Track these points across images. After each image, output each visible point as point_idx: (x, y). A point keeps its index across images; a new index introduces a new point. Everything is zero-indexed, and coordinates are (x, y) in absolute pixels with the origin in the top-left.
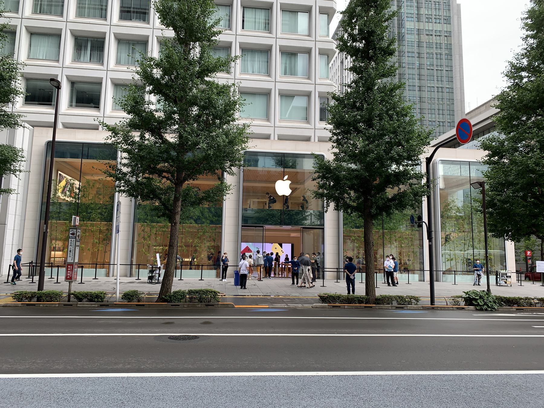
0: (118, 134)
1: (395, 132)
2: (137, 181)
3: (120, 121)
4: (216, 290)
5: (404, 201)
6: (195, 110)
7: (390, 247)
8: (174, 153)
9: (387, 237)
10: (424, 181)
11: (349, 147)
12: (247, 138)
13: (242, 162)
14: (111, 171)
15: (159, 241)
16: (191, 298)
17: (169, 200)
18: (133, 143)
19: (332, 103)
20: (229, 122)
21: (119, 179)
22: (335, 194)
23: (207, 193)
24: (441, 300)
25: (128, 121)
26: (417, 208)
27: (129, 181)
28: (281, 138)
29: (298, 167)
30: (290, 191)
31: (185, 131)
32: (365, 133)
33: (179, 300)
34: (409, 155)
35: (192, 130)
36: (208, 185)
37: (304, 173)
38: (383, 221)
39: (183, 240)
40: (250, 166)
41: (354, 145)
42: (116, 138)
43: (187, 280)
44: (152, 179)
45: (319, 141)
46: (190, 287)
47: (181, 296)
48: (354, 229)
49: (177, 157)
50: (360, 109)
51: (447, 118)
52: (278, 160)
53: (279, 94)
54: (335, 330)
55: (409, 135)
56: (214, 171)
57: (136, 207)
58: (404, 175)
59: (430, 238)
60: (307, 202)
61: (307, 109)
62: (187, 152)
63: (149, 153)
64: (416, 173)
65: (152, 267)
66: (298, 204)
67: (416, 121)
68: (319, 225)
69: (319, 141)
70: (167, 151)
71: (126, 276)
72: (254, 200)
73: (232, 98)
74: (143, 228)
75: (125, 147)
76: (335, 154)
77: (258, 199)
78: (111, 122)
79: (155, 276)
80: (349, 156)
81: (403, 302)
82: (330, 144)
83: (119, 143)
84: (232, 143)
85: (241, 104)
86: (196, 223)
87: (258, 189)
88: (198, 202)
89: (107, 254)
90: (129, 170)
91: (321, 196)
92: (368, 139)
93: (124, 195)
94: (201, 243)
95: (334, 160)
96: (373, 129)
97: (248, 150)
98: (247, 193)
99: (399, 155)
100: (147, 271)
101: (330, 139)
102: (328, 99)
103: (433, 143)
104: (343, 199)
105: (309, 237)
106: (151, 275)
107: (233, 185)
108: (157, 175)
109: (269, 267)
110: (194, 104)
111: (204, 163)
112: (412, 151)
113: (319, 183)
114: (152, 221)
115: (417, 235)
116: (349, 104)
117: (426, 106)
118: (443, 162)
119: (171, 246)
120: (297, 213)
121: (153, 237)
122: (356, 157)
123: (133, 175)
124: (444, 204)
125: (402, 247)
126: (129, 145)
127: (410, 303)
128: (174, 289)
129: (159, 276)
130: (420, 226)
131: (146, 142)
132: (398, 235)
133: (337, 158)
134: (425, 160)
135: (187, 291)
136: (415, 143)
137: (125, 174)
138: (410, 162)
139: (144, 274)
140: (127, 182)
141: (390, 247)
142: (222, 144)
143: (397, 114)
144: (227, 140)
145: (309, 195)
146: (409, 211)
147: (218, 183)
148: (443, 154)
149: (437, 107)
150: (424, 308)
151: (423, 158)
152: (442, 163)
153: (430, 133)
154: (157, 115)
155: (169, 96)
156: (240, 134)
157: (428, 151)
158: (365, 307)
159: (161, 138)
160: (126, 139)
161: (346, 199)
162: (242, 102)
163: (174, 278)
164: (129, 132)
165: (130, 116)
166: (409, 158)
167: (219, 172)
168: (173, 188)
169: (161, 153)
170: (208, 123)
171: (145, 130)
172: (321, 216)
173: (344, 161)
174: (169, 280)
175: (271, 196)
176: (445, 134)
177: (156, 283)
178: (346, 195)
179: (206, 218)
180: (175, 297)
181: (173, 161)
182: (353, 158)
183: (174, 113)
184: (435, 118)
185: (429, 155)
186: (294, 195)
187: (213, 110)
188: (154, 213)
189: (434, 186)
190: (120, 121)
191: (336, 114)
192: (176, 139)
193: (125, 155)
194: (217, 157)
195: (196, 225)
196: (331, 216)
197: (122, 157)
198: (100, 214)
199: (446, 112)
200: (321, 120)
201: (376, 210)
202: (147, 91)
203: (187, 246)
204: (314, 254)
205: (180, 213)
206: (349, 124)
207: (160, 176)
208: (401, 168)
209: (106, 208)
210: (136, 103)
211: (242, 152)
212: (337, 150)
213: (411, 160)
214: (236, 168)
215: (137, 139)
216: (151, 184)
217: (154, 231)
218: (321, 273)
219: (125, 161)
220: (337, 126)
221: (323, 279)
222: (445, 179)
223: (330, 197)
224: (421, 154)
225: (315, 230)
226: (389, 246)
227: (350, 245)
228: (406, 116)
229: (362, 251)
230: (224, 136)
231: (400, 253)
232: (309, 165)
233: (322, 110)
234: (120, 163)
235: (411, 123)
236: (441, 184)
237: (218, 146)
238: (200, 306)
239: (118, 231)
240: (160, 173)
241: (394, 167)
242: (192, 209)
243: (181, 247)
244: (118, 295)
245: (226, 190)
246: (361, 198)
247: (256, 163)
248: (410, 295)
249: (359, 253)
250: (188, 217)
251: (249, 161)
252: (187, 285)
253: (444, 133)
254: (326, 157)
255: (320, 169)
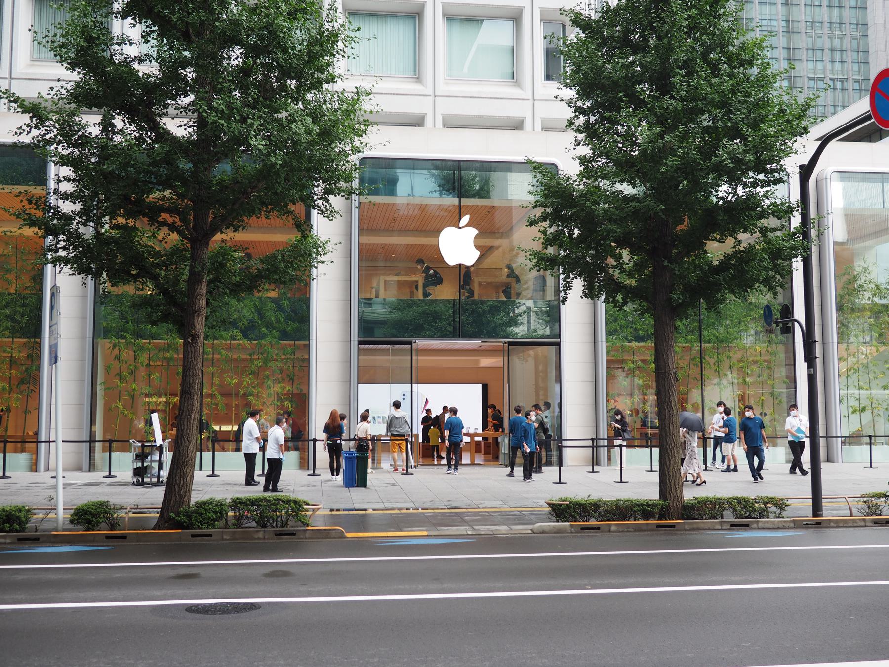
0: (48, 119)
1: (724, 104)
2: (98, 235)
3: (52, 89)
4: (301, 497)
5: (748, 272)
6: (235, 57)
7: (719, 384)
8: (185, 165)
9: (710, 360)
10: (796, 221)
11: (616, 141)
12: (367, 123)
13: (355, 184)
14: (33, 212)
15: (157, 383)
16: (239, 518)
17: (176, 281)
18: (85, 141)
19: (574, 34)
20: (321, 84)
21: (53, 231)
22: (584, 258)
23: (270, 260)
24: (836, 506)
25: (70, 86)
26: (778, 288)
27: (78, 236)
28: (451, 124)
29: (493, 194)
30: (476, 254)
31: (211, 108)
32: (653, 107)
33: (211, 522)
34: (758, 158)
35: (229, 106)
36: (274, 244)
37: (508, 210)
38: (700, 321)
39: (217, 381)
40: (376, 193)
41: (629, 137)
42: (43, 131)
43: (219, 478)
44: (135, 229)
45: (545, 129)
46: (237, 491)
47: (216, 513)
48: (633, 344)
49: (195, 174)
50: (640, 48)
51: (853, 71)
52: (444, 178)
53: (444, 15)
54: (586, 581)
55: (758, 111)
56: (286, 205)
57: (98, 300)
58: (747, 209)
59: (810, 359)
60: (518, 280)
61: (514, 52)
62: (218, 161)
63: (126, 165)
64: (775, 204)
65: (143, 446)
66: (496, 286)
67: (774, 76)
68: (548, 337)
69: (545, 129)
70: (169, 160)
71: (79, 469)
72: (388, 278)
73: (327, 25)
74: (116, 352)
75: (65, 152)
76: (583, 160)
77: (397, 274)
78: (28, 92)
79: (150, 467)
80: (617, 163)
81: (747, 513)
82: (570, 136)
83: (49, 142)
84: (328, 135)
85: (348, 39)
86: (246, 336)
87: (395, 252)
88: (249, 283)
89: (31, 418)
90: (78, 207)
91: (550, 263)
92: (661, 120)
93: (67, 269)
94: (261, 385)
95: (581, 175)
96: (672, 97)
97: (368, 153)
98: (370, 262)
99: (735, 160)
100: (130, 456)
101: (571, 123)
102: (564, 26)
103: (819, 130)
104: (604, 269)
105: (524, 366)
106: (140, 465)
107: (333, 241)
108: (145, 220)
109: (438, 441)
110: (232, 41)
111: (260, 185)
112: (765, 149)
113: (544, 232)
114: (139, 335)
115: (782, 356)
116: (612, 37)
117: (801, 41)
118: (845, 175)
119: (186, 393)
120: (495, 309)
121: (142, 372)
122: (633, 165)
123: (88, 220)
124: (845, 278)
125: (745, 382)
126: (74, 146)
127: (763, 513)
128: (196, 497)
129: (161, 467)
130: (788, 330)
131: (117, 139)
132: (736, 355)
133: (588, 169)
134: (797, 170)
135: (228, 501)
136: (772, 131)
137: (68, 219)
138: (761, 177)
139: (124, 464)
140: (74, 238)
141: (719, 384)
142: (304, 138)
143: (730, 60)
144: (316, 129)
145: (523, 262)
146: (761, 297)
147: (293, 237)
148: (840, 156)
149: (827, 45)
150: (799, 525)
151: (792, 164)
152: (842, 179)
153: (809, 106)
154: (142, 69)
155: (169, 21)
156: (348, 113)
157: (803, 148)
158: (659, 526)
159: (155, 126)
160: (69, 131)
161: (611, 271)
162: (352, 34)
163: (197, 473)
164: (73, 114)
165: (75, 76)
166: (759, 167)
167: (298, 208)
168: (186, 250)
169: (154, 164)
170: (268, 87)
171: (114, 109)
172: (553, 316)
173: (605, 177)
174: (185, 476)
175: (428, 268)
176: (847, 110)
177: (155, 485)
178: (611, 261)
179: (269, 325)
180: (201, 514)
181: (185, 182)
182: (627, 168)
183: (185, 64)
184: (824, 70)
185: (805, 160)
186: (486, 264)
187: (280, 55)
188: (142, 313)
189: (820, 235)
190: (52, 89)
191: (584, 62)
192: (190, 130)
193: (66, 171)
194: (293, 170)
195: (246, 343)
196: (578, 314)
197: (60, 177)
198: (11, 318)
199: (849, 56)
200: (548, 77)
201: (682, 293)
202: (115, 10)
203: (226, 394)
204: (537, 407)
205: (205, 312)
206: (615, 85)
207: (153, 220)
208: (740, 191)
209: (24, 305)
210: (90, 40)
211: (354, 158)
212: (586, 151)
213: (766, 172)
214: (339, 197)
215: (95, 131)
216: (132, 242)
217: (143, 358)
218: (555, 453)
219: (67, 187)
220: (585, 91)
221: (560, 464)
222: (851, 218)
223: (572, 266)
224: (787, 155)
225: (540, 349)
226: (716, 381)
227: (623, 381)
228: (751, 63)
229: (652, 398)
230: (309, 120)
231: (742, 398)
232: (520, 190)
233: (550, 55)
234: (56, 191)
235: (764, 81)
236: (836, 230)
237: (295, 144)
238: (261, 535)
239: (54, 359)
240: (152, 213)
241: (724, 189)
242: (233, 302)
243: (212, 396)
244: (62, 515)
245: (317, 253)
246: (646, 267)
247: (391, 186)
248: (764, 495)
249: (644, 401)
250: (224, 322)
251: (372, 181)
252: (229, 488)
253: (844, 107)
254: (560, 167)
255: (546, 196)
